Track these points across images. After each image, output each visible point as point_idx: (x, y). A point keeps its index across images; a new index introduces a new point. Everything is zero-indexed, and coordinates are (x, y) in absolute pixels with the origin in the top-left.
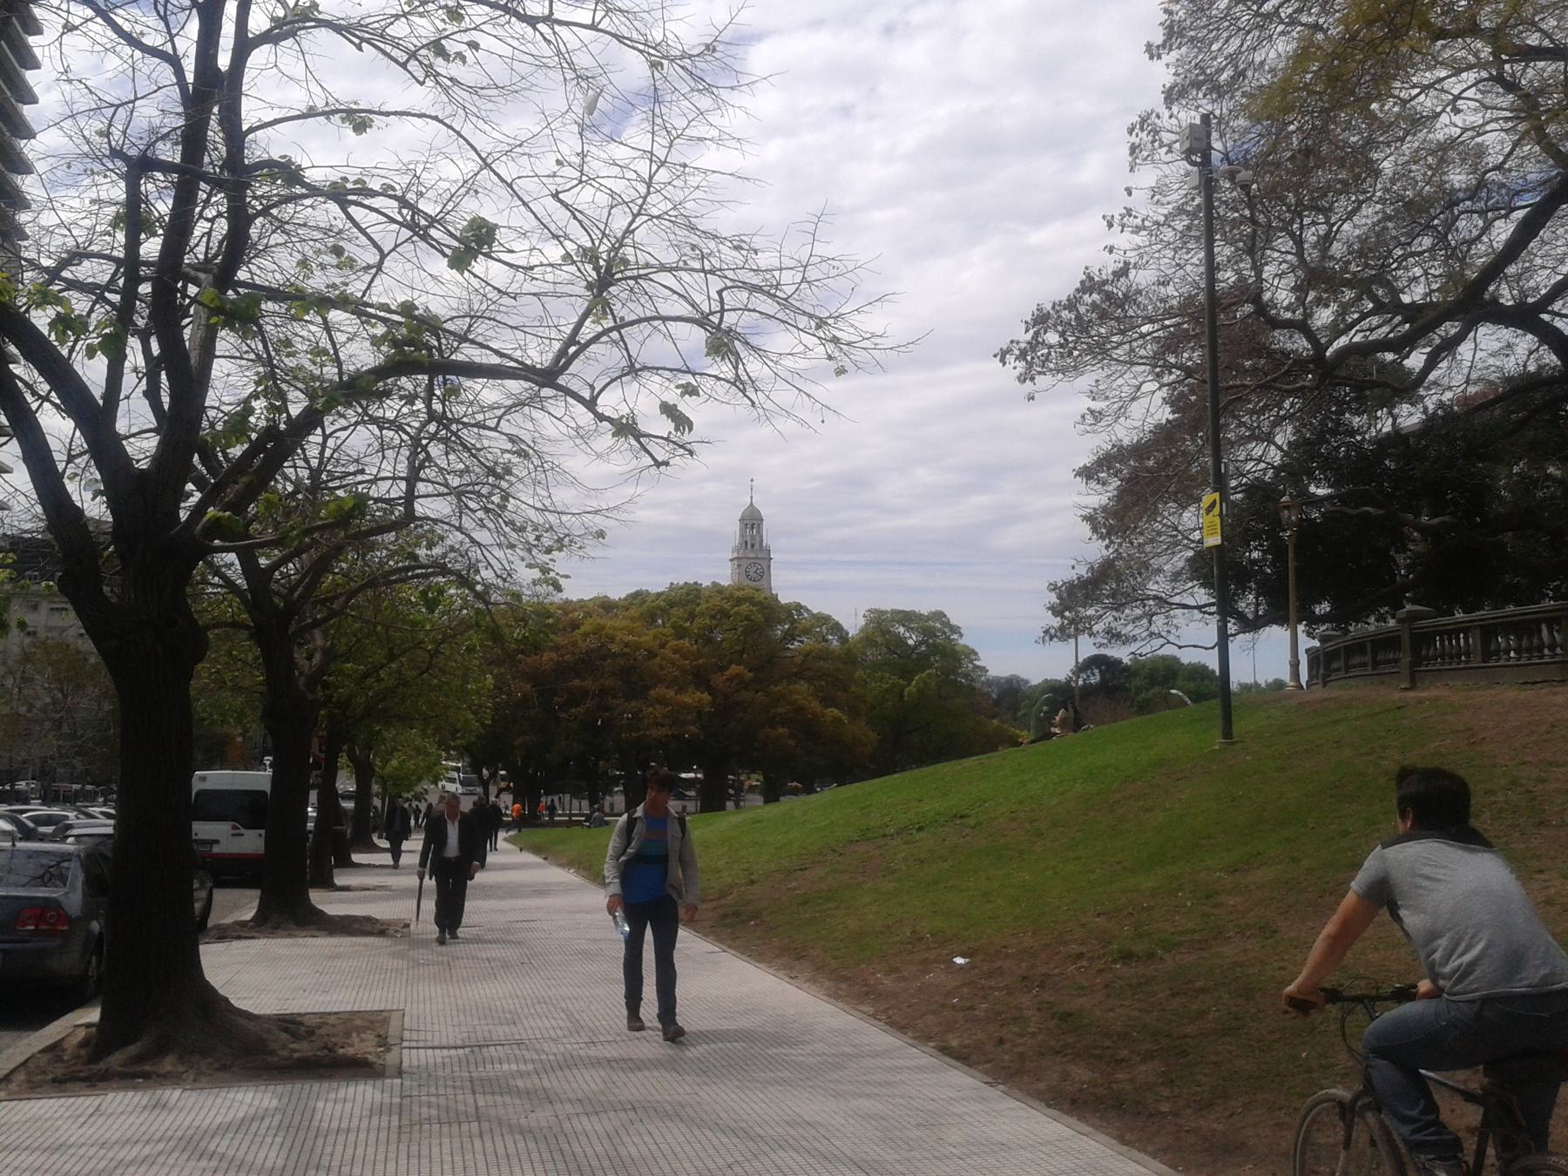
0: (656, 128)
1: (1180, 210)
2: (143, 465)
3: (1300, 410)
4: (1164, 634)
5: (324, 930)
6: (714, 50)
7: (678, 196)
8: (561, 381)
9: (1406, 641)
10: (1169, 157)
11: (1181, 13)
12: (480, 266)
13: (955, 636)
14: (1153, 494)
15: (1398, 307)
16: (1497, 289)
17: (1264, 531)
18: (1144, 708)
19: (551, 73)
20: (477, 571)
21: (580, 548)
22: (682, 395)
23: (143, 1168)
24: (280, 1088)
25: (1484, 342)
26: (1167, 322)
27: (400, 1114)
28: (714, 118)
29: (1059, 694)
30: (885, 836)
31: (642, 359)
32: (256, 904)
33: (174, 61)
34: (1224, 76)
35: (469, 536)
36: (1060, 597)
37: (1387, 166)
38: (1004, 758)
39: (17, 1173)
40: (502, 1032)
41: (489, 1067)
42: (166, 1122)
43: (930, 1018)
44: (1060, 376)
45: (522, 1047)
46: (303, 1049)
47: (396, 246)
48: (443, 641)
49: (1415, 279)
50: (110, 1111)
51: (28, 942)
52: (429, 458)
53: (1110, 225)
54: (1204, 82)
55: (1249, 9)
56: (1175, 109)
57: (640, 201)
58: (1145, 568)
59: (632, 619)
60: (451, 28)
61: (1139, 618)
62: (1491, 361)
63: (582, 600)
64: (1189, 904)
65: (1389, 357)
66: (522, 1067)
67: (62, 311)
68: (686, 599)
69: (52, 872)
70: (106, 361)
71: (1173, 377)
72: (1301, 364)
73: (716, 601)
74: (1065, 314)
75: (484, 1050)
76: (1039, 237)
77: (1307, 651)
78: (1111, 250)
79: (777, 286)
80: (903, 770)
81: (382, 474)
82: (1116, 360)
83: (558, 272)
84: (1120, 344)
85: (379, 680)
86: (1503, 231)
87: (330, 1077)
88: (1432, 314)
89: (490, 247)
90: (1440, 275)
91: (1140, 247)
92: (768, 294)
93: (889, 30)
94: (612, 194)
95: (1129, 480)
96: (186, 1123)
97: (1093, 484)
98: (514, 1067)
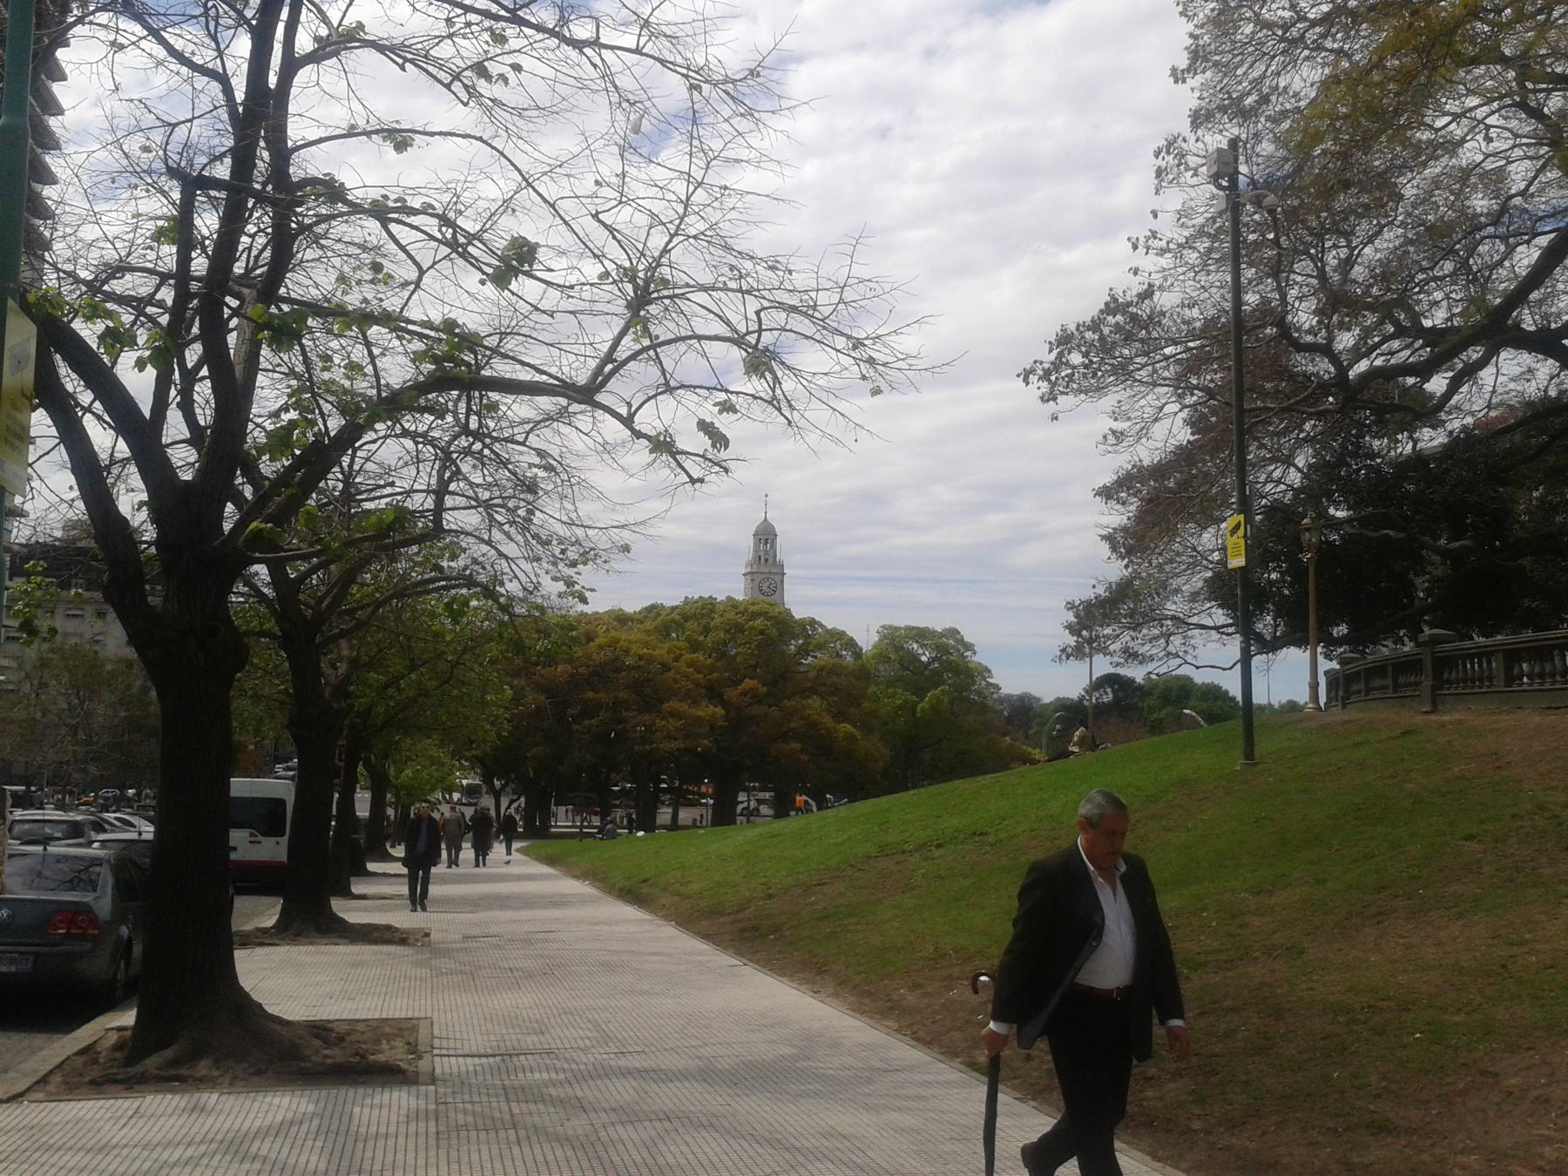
0: (694, 150)
1: (1201, 233)
2: (187, 476)
3: (1321, 433)
4: (1181, 654)
5: (345, 938)
6: (758, 75)
7: (714, 216)
8: (599, 398)
9: (1428, 663)
10: (1195, 181)
11: (1205, 38)
12: (520, 284)
13: (969, 653)
14: (1176, 514)
15: (1421, 332)
16: (1520, 313)
17: (1284, 554)
18: (1157, 728)
19: (596, 97)
20: (502, 584)
21: (605, 562)
22: (720, 412)
23: (188, 1169)
24: (316, 1093)
25: (1505, 366)
26: (1191, 344)
27: (437, 1120)
28: (754, 140)
29: (1072, 713)
30: (903, 852)
31: (680, 375)
32: (279, 907)
33: (223, 80)
34: (1249, 101)
35: (496, 549)
36: (1077, 616)
37: (1409, 192)
38: (1016, 775)
39: (64, 1172)
40: (530, 1041)
41: (521, 1075)
42: (207, 1124)
43: (956, 1035)
44: (1083, 396)
45: (553, 1056)
46: (337, 1055)
47: (435, 263)
48: (464, 652)
49: (1436, 303)
50: (150, 1112)
51: (60, 945)
52: (459, 471)
53: (1135, 247)
54: (1229, 107)
55: (1274, 34)
56: (1200, 132)
57: (677, 222)
58: (1163, 589)
59: (647, 631)
60: (493, 51)
61: (1156, 638)
62: (1512, 385)
63: (597, 613)
64: (1214, 924)
65: (1411, 381)
66: (553, 1076)
67: (111, 325)
68: (699, 613)
69: (82, 874)
70: (154, 372)
71: (1195, 398)
72: (1324, 388)
73: (731, 615)
74: (1089, 335)
75: (515, 1059)
76: (1068, 258)
77: (1326, 673)
78: (1136, 272)
79: (815, 307)
80: (914, 787)
81: (416, 487)
82: (1140, 381)
83: (595, 290)
84: (1144, 366)
85: (399, 690)
86: (1526, 257)
87: (363, 1083)
88: (1456, 339)
89: (531, 266)
90: (1461, 300)
91: (1164, 270)
92: (805, 314)
93: (929, 54)
94: (652, 214)
95: (1150, 501)
96: (226, 1126)
97: (1112, 503)
98: (553, 1076)
